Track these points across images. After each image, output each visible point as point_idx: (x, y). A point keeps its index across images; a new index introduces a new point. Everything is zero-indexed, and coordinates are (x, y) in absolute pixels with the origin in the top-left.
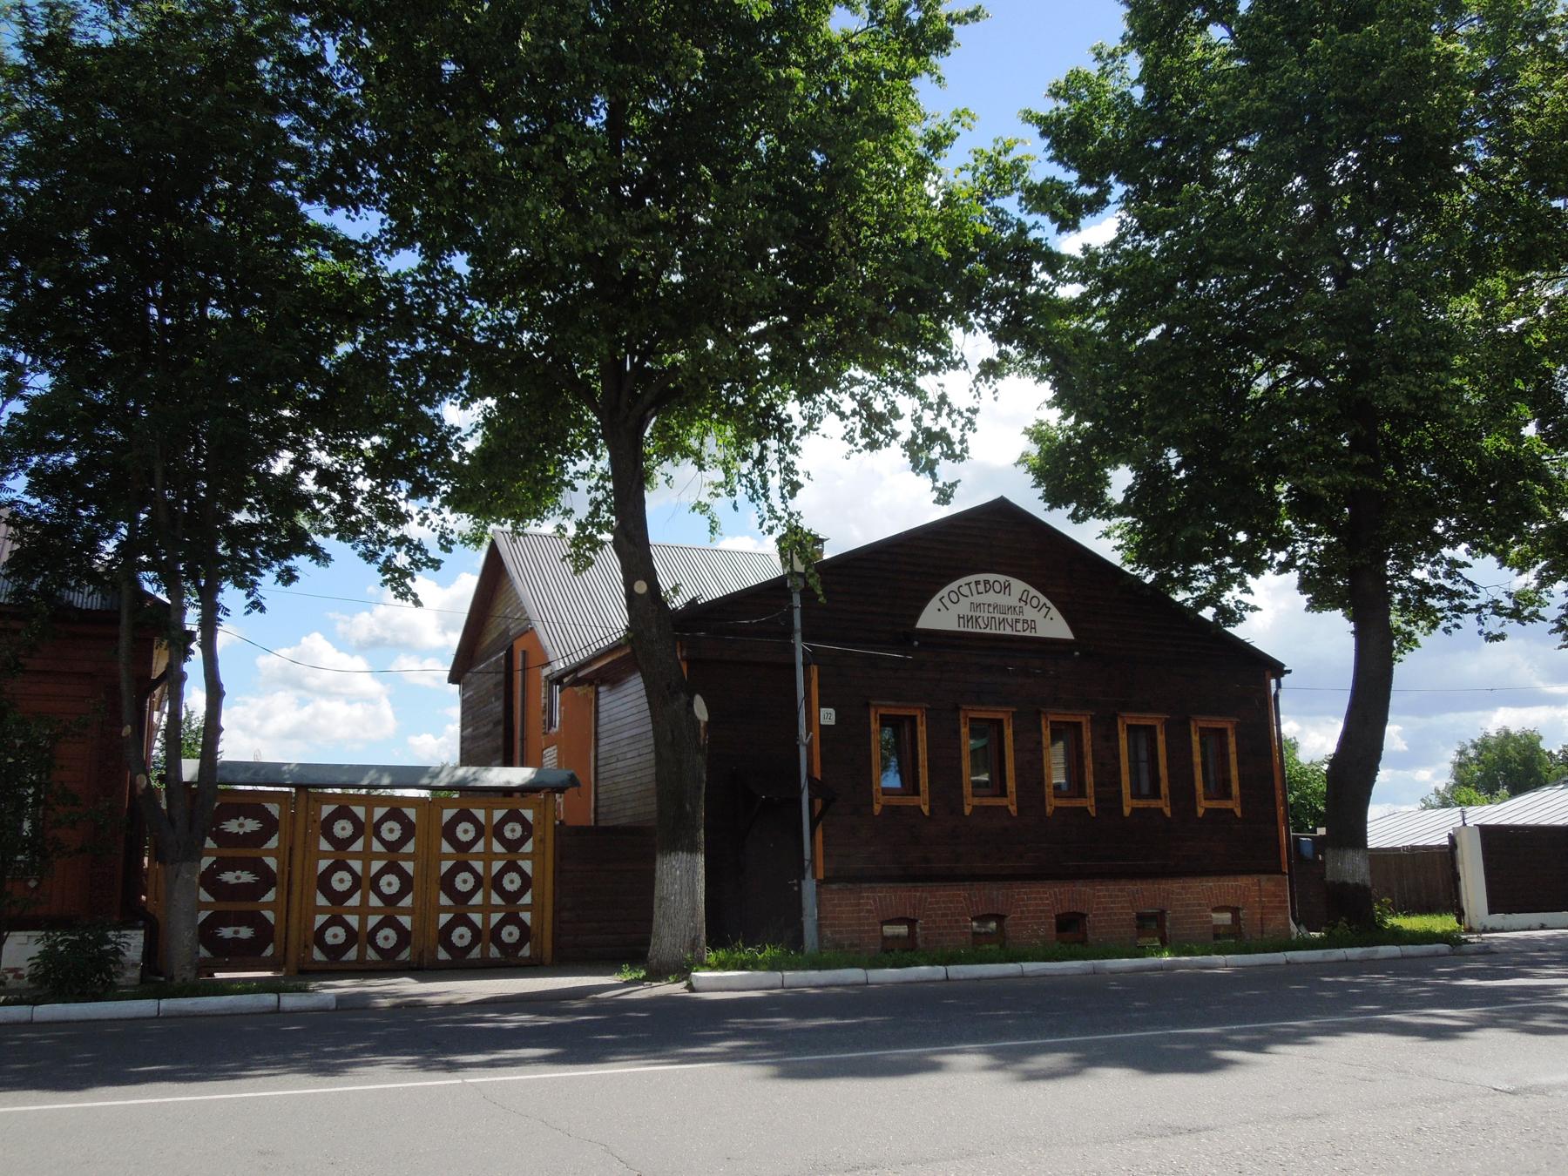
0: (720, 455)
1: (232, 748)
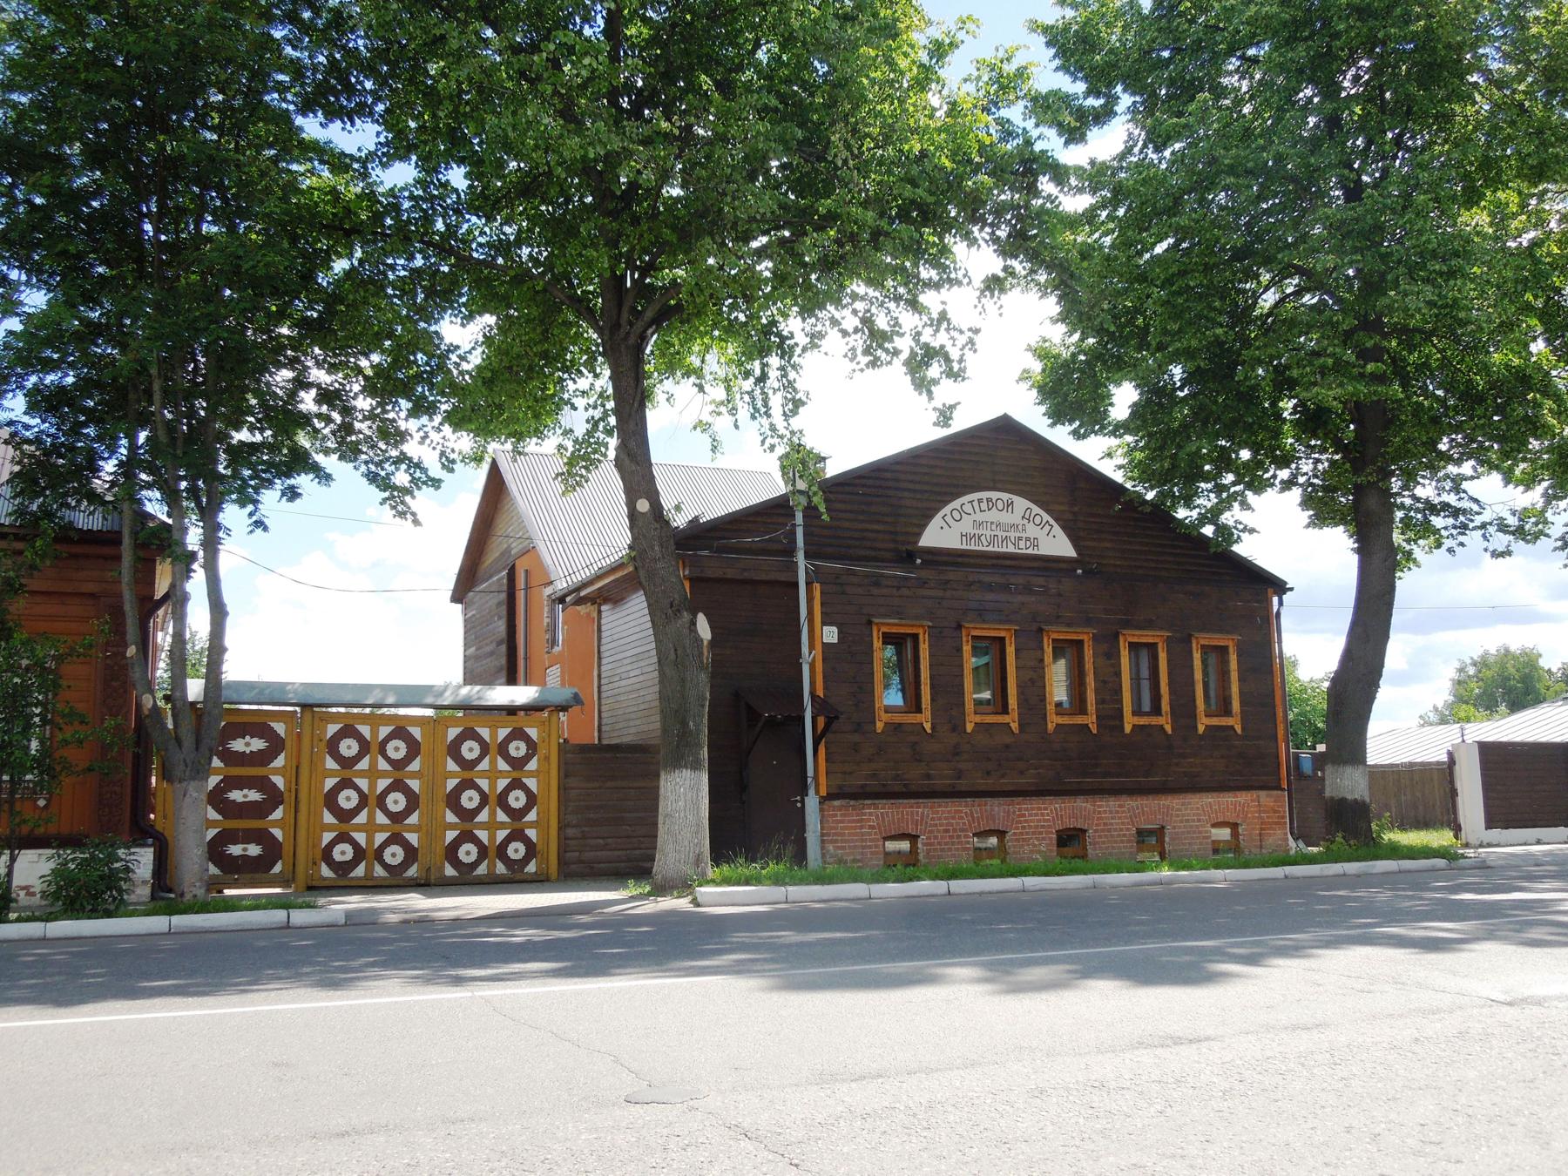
0: (721, 374)
1: (235, 670)
